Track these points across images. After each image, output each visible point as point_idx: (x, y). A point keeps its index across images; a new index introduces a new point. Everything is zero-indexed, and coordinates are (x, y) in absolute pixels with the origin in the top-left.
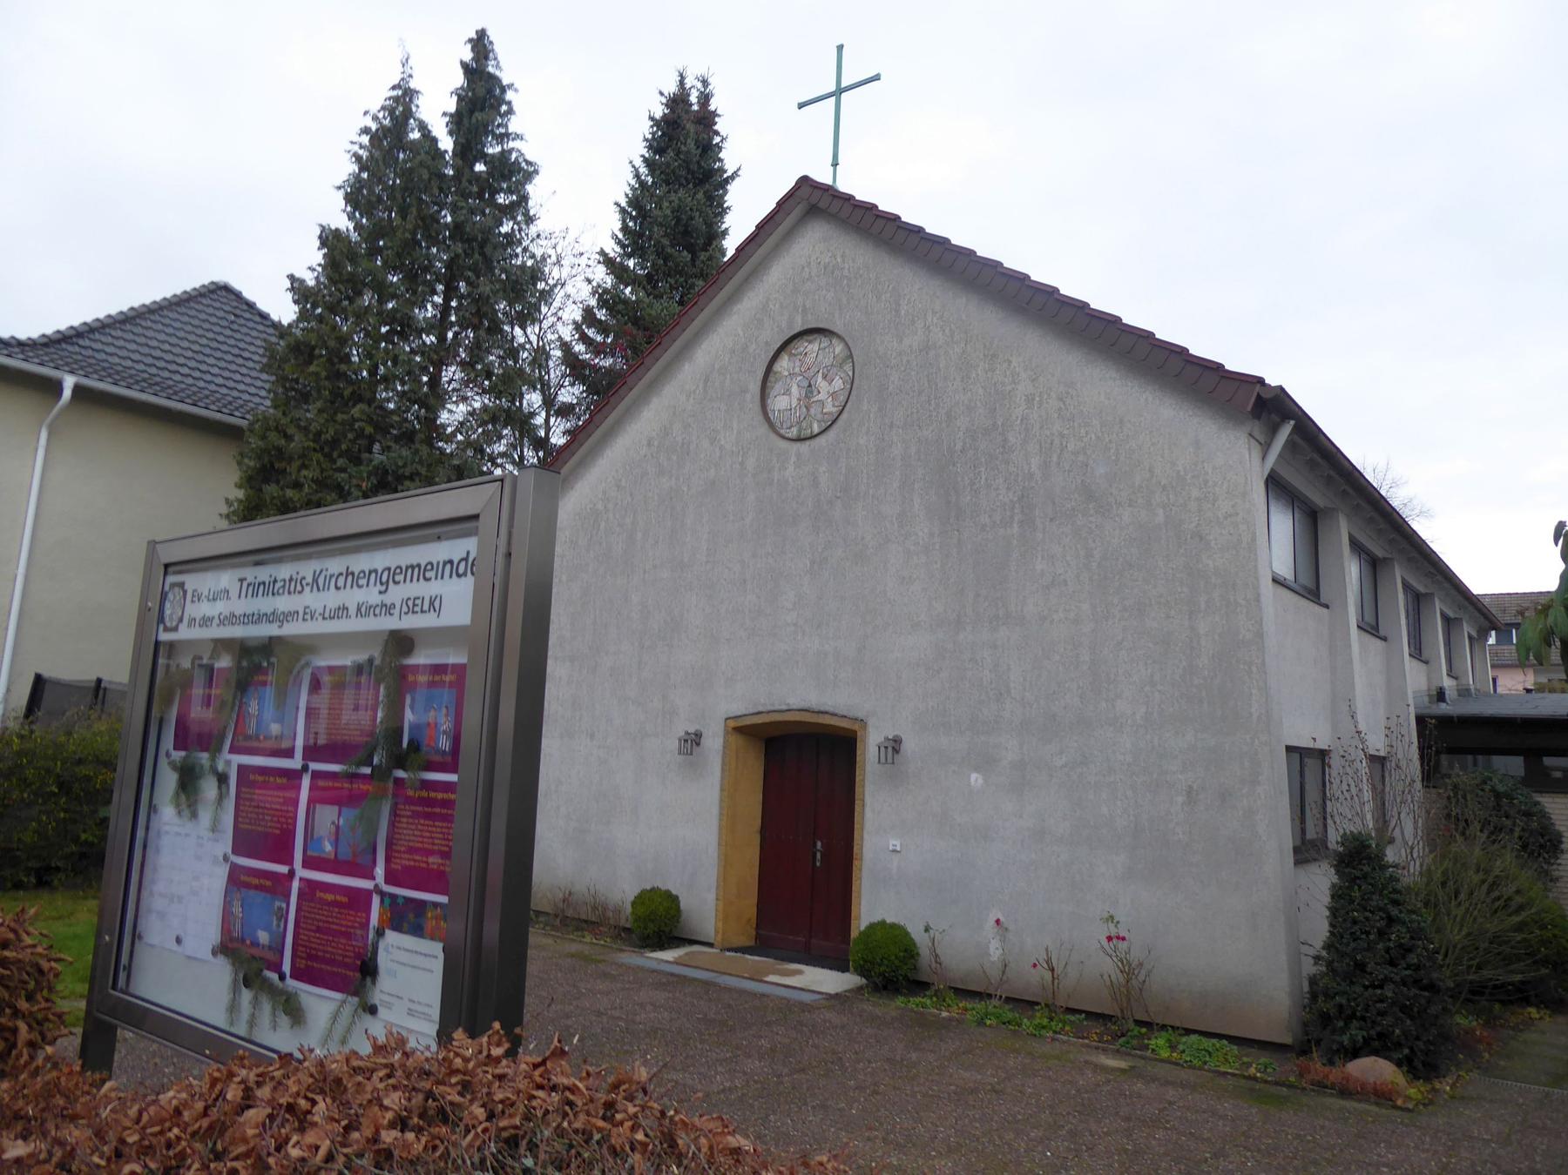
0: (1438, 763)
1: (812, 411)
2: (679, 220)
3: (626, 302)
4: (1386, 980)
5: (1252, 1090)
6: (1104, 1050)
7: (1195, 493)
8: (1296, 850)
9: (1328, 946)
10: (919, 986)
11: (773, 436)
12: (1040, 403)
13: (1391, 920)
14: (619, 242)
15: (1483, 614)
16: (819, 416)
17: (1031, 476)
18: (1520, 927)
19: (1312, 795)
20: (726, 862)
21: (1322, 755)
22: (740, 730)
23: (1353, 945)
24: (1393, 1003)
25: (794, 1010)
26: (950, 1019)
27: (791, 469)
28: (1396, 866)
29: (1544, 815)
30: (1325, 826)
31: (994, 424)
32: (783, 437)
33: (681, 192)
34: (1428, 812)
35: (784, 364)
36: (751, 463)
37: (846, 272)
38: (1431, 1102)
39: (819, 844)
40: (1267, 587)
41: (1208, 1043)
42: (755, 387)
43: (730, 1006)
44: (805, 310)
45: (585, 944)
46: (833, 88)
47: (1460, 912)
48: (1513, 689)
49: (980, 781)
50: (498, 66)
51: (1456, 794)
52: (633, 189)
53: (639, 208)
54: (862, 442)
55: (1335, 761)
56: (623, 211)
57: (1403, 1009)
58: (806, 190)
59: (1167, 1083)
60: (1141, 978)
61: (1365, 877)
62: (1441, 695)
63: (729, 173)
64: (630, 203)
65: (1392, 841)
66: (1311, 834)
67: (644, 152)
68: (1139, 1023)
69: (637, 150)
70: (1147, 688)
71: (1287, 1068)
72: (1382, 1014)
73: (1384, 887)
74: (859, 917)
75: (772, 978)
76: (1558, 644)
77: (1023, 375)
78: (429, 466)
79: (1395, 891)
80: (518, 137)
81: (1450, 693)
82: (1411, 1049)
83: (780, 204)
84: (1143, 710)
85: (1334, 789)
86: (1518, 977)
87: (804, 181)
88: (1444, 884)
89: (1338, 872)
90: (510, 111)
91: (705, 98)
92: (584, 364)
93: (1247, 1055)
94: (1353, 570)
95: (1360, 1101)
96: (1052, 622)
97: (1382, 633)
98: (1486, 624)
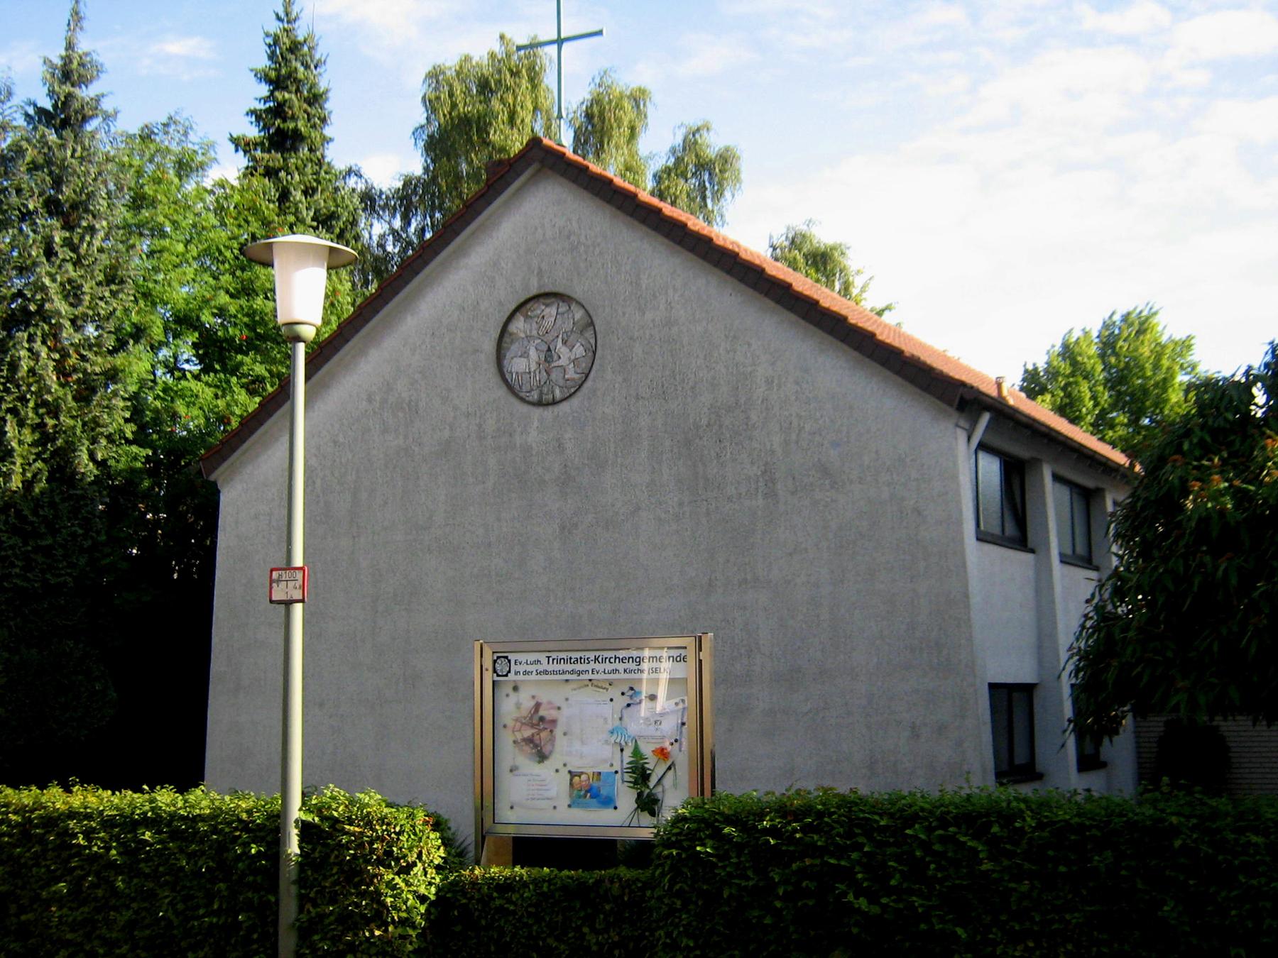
1: (553, 376)
11: (513, 400)
12: (779, 386)
16: (561, 382)
21: (1027, 690)
32: (522, 400)
35: (519, 325)
42: (489, 346)
54: (607, 411)
84: (875, 660)
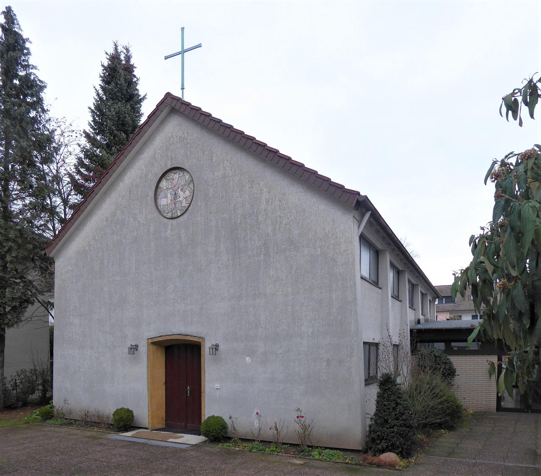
0: (416, 347)
1: (177, 206)
2: (119, 118)
3: (97, 156)
4: (395, 425)
5: (347, 468)
6: (295, 457)
7: (332, 242)
8: (366, 380)
9: (375, 415)
10: (228, 439)
12: (272, 202)
13: (397, 404)
14: (92, 127)
15: (435, 292)
17: (268, 234)
18: (440, 403)
19: (373, 360)
20: (151, 397)
21: (377, 345)
22: (154, 343)
23: (384, 414)
24: (397, 433)
25: (178, 453)
26: (239, 451)
27: (169, 232)
28: (400, 384)
29: (451, 363)
30: (377, 371)
31: (253, 212)
33: (119, 104)
34: (412, 364)
35: (164, 184)
36: (152, 229)
37: (189, 141)
38: (408, 466)
39: (188, 387)
40: (358, 280)
41: (332, 452)
42: (151, 194)
43: (152, 453)
44: (172, 158)
45: (94, 432)
46: (180, 50)
47: (421, 399)
48: (442, 319)
49: (250, 360)
50: (20, 28)
51: (422, 357)
52: (96, 101)
53: (99, 111)
54: (198, 219)
55: (381, 347)
56: (92, 111)
57: (400, 435)
58: (169, 100)
59: (317, 468)
60: (309, 430)
61: (389, 389)
62: (419, 322)
63: (142, 97)
64: (96, 108)
65: (399, 375)
66: (371, 375)
67: (101, 83)
68: (309, 446)
69: (98, 82)
70: (313, 322)
71: (362, 456)
72: (393, 437)
73: (396, 392)
74: (204, 415)
75: (170, 440)
76: (471, 287)
77: (265, 190)
78: (6, 229)
79: (399, 393)
80: (34, 67)
81: (422, 321)
82: (402, 448)
83: (158, 106)
85: (381, 357)
86: (438, 421)
87: (168, 95)
88: (416, 390)
89: (380, 388)
90: (29, 53)
91: (128, 58)
92: (83, 186)
93: (346, 455)
94: (391, 275)
95: (384, 468)
96: (277, 296)
97: (400, 299)
98: (436, 296)
